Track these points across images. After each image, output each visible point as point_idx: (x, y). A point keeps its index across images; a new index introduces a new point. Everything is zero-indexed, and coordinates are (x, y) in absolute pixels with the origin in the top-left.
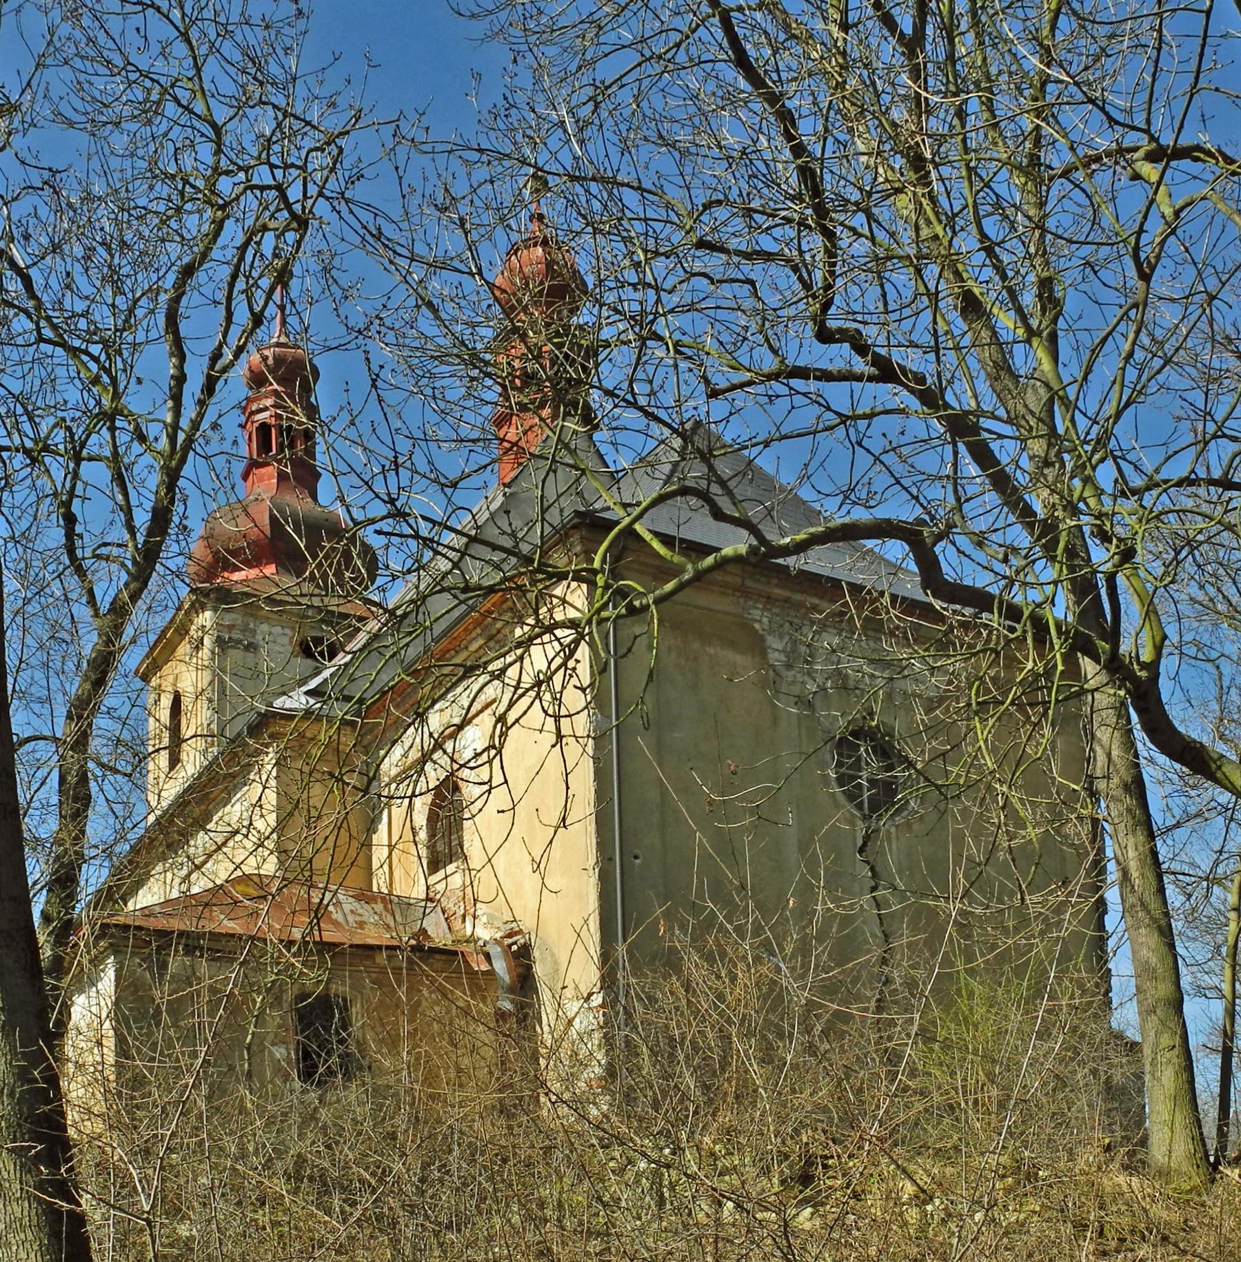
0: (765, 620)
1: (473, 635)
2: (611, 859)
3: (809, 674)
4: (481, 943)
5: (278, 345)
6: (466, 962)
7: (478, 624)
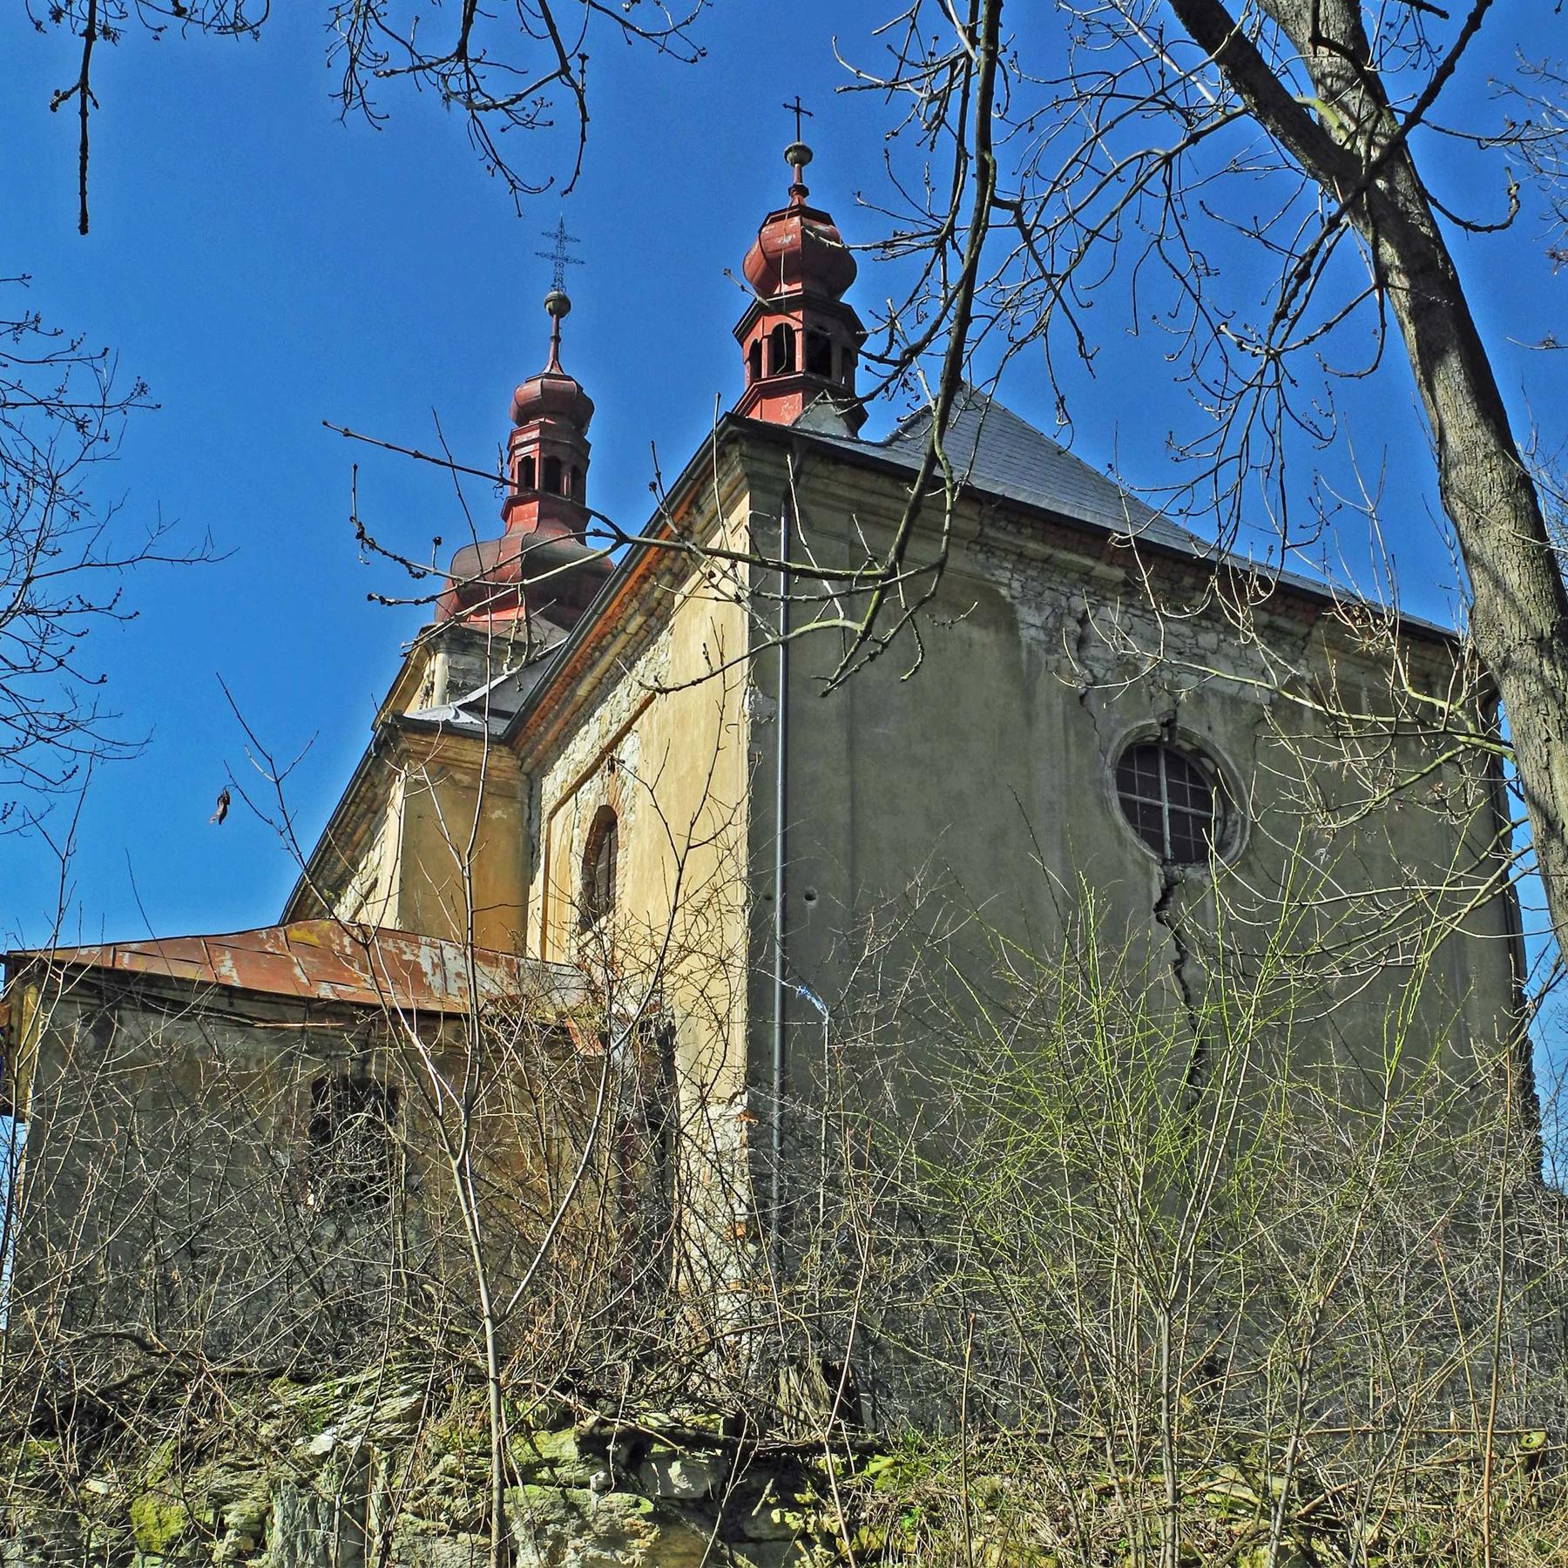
0: (1016, 584)
1: (630, 611)
2: (770, 898)
5: (549, 376)
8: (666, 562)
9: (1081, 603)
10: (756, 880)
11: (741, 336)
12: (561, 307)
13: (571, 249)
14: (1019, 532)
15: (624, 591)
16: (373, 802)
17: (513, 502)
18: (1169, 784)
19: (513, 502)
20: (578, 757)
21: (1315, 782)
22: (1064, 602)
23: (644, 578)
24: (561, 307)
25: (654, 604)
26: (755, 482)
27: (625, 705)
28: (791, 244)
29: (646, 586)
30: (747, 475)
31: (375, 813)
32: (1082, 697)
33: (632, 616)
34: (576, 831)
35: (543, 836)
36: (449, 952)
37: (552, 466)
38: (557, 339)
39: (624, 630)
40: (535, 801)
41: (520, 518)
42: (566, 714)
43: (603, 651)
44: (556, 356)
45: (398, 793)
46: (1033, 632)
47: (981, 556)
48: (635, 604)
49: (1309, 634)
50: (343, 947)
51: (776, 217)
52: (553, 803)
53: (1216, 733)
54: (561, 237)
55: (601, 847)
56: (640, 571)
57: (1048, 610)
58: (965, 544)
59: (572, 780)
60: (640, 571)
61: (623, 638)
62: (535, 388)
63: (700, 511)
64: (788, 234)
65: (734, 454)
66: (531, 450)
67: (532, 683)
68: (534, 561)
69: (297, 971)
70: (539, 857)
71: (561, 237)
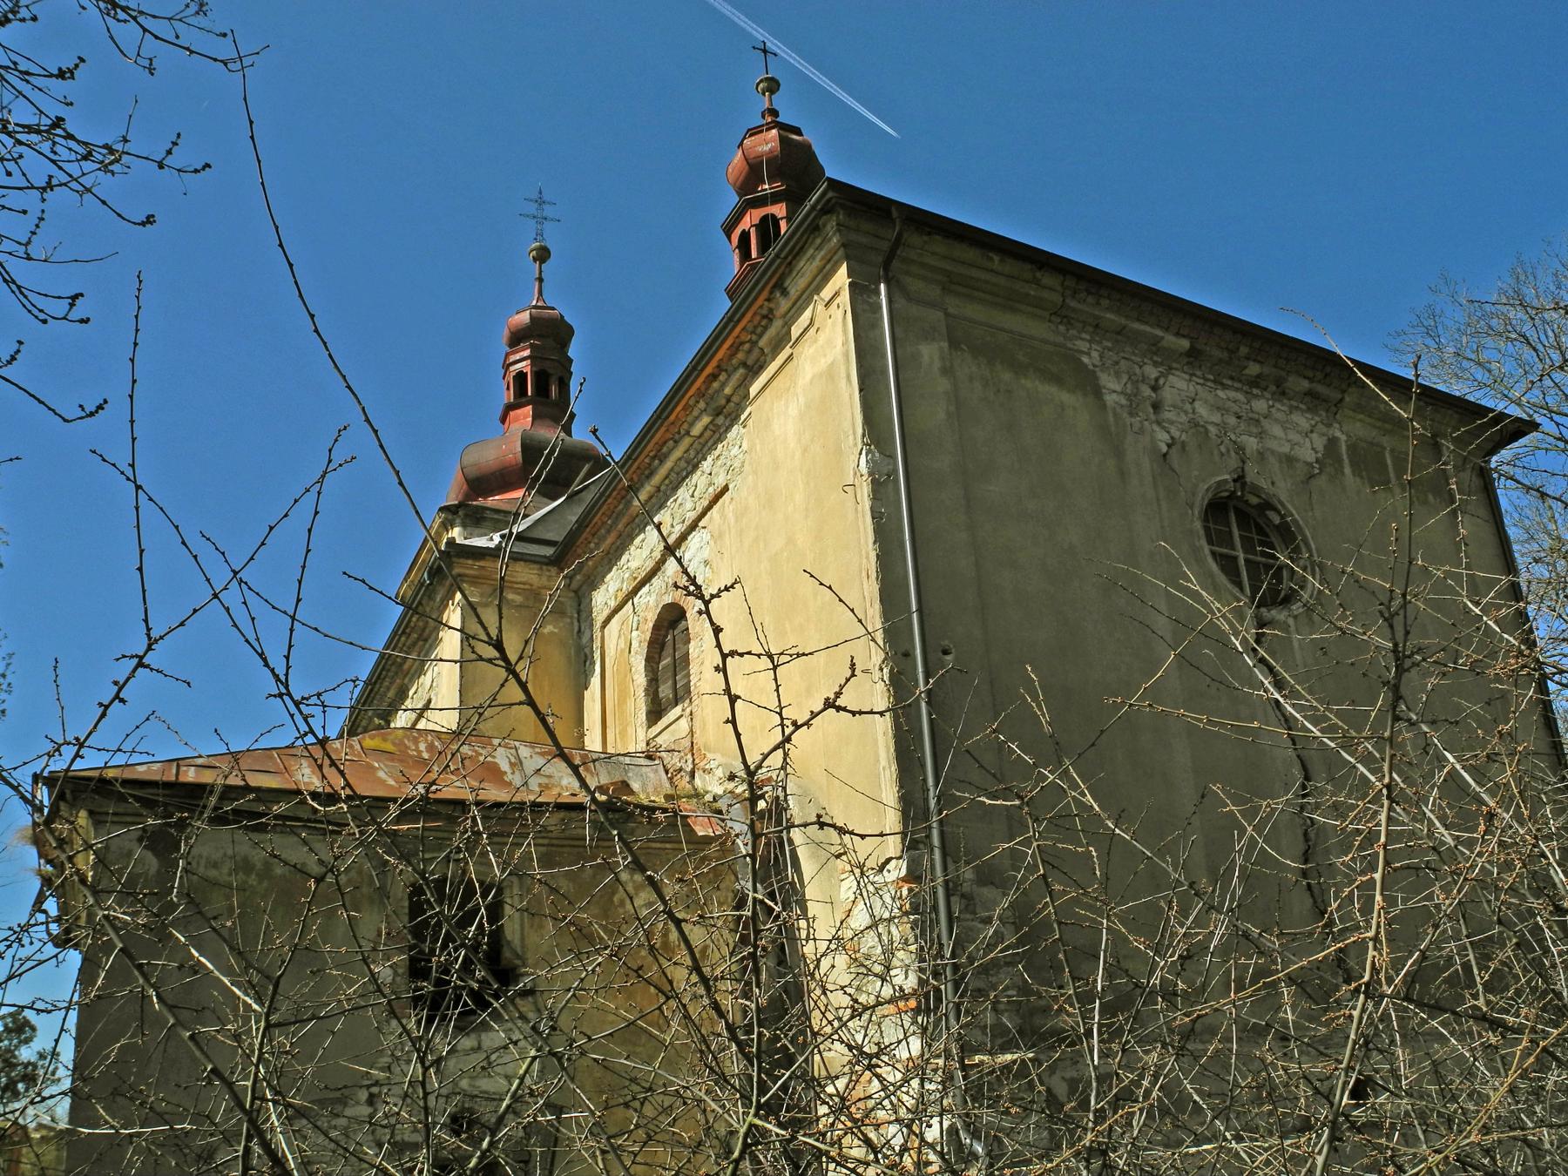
0: (1095, 354)
1: (695, 413)
2: (908, 655)
3: (1159, 423)
4: (708, 798)
5: (535, 307)
6: (686, 826)
7: (701, 394)
8: (740, 356)
9: (1152, 372)
10: (895, 636)
11: (728, 231)
12: (543, 255)
13: (548, 211)
14: (1098, 304)
15: (691, 393)
16: (423, 630)
17: (510, 407)
18: (1241, 536)
19: (510, 407)
20: (633, 565)
21: (1352, 529)
22: (1138, 370)
23: (714, 377)
24: (543, 255)
25: (723, 402)
26: (853, 255)
27: (689, 505)
28: (771, 151)
29: (716, 385)
30: (844, 245)
31: (426, 640)
32: (1165, 455)
33: (697, 418)
34: (635, 634)
35: (597, 644)
36: (524, 752)
37: (542, 379)
38: (540, 280)
39: (688, 433)
40: (584, 615)
41: (517, 419)
42: (620, 526)
43: (662, 459)
44: (540, 293)
45: (454, 616)
46: (1114, 396)
47: (1062, 328)
48: (702, 405)
49: (1341, 400)
50: (420, 752)
51: (755, 131)
52: (606, 613)
53: (1281, 489)
54: (541, 202)
55: (663, 646)
56: (709, 370)
57: (1125, 378)
58: (1046, 314)
59: (627, 587)
60: (709, 370)
61: (687, 441)
62: (525, 317)
63: (785, 293)
64: (769, 142)
65: (830, 225)
66: (524, 366)
67: (573, 517)
68: (531, 450)
69: (381, 774)
70: (593, 663)
71: (541, 202)
